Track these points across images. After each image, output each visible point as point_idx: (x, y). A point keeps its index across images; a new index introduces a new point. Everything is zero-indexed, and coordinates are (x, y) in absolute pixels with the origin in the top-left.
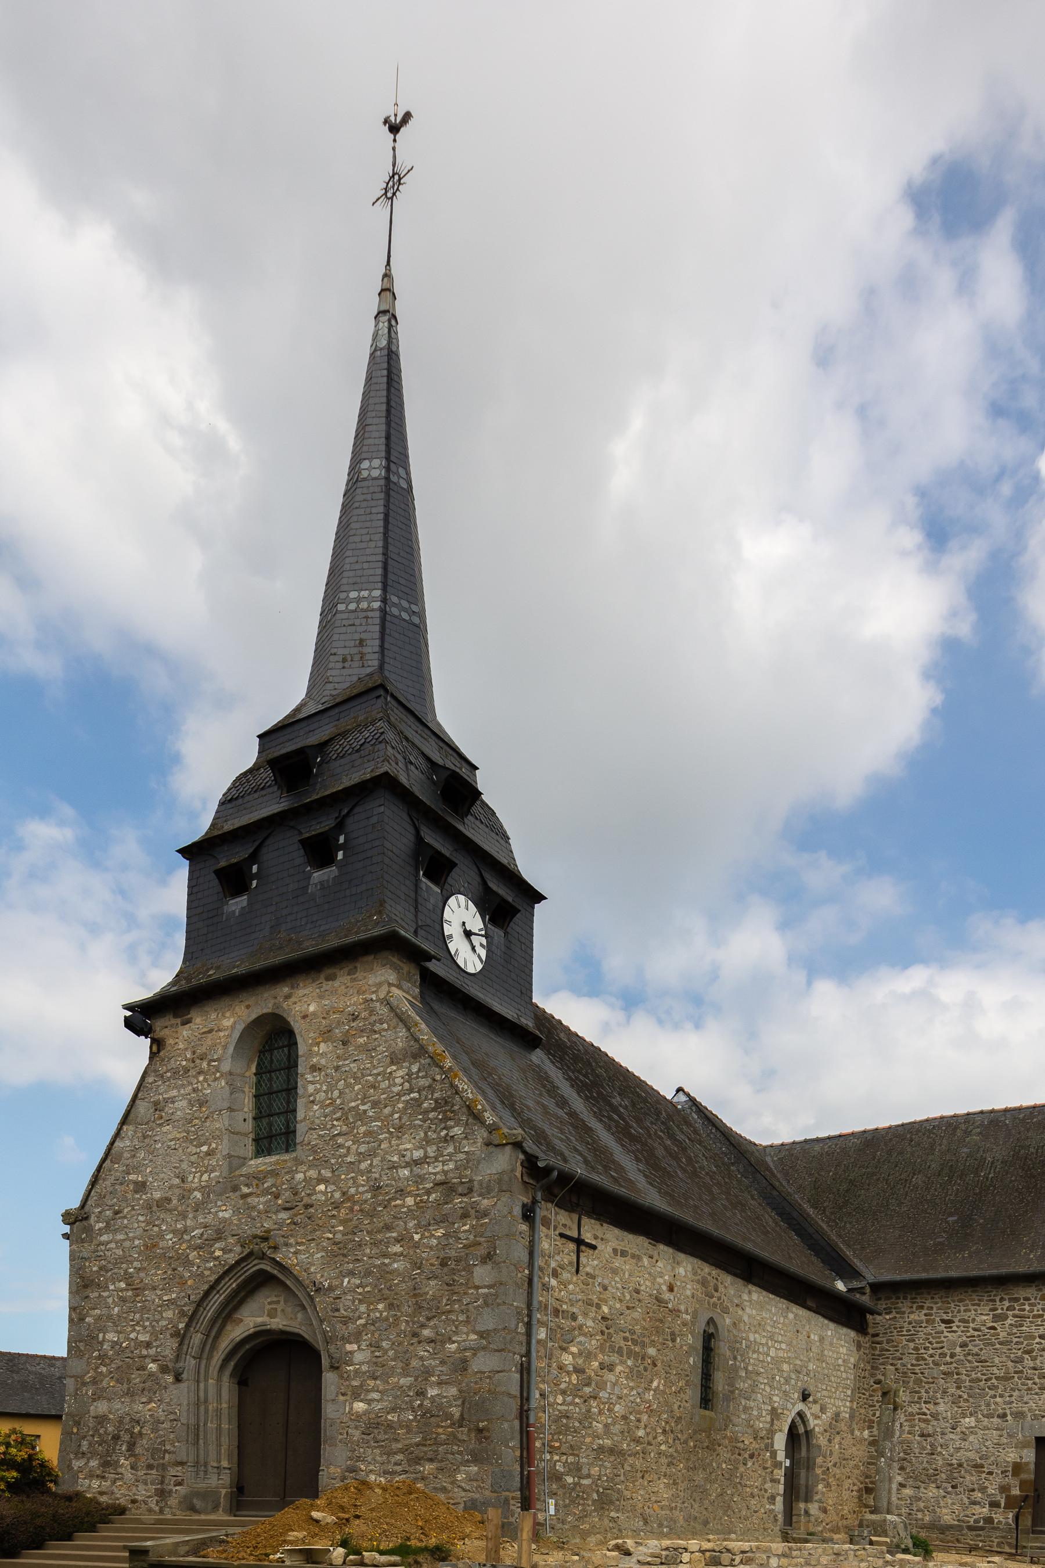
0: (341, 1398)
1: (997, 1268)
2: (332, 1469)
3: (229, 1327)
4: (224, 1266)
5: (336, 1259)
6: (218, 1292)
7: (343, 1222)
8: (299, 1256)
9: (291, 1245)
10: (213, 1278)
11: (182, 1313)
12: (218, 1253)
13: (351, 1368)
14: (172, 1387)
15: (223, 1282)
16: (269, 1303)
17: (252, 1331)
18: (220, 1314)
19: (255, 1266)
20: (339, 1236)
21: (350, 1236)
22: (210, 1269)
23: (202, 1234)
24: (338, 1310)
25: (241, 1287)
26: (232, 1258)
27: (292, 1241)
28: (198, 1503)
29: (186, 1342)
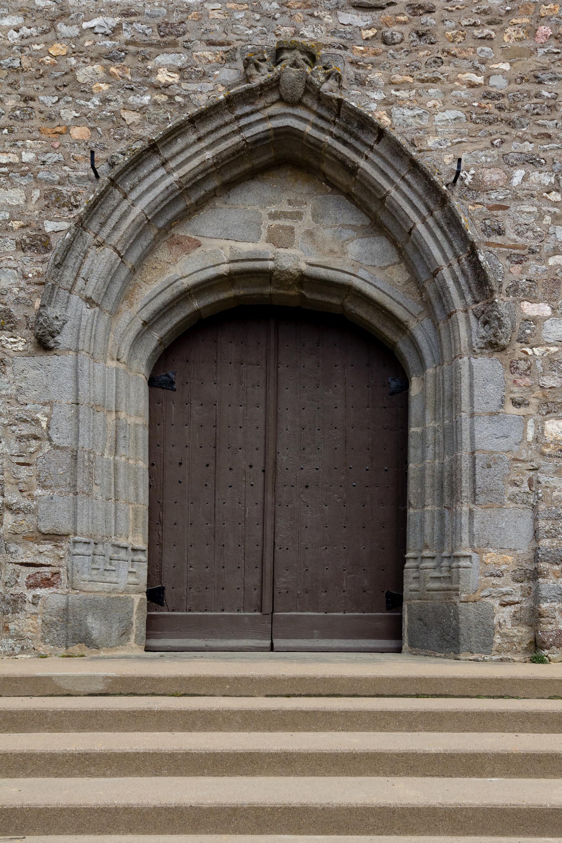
0: (511, 409)
1: (111, 485)
2: (491, 556)
3: (163, 254)
4: (182, 107)
5: (492, 129)
6: (164, 164)
7: (511, 55)
8: (395, 110)
9: (373, 85)
10: (151, 132)
11: (55, 200)
12: (163, 77)
13: (537, 351)
14: (21, 363)
15: (180, 143)
16: (274, 216)
17: (224, 269)
18: (157, 216)
19: (274, 117)
20: (498, 83)
21: (526, 86)
22: (142, 109)
23: (117, 29)
24: (500, 232)
25: (221, 164)
26: (204, 94)
27: (376, 75)
28: (95, 625)
29: (71, 262)
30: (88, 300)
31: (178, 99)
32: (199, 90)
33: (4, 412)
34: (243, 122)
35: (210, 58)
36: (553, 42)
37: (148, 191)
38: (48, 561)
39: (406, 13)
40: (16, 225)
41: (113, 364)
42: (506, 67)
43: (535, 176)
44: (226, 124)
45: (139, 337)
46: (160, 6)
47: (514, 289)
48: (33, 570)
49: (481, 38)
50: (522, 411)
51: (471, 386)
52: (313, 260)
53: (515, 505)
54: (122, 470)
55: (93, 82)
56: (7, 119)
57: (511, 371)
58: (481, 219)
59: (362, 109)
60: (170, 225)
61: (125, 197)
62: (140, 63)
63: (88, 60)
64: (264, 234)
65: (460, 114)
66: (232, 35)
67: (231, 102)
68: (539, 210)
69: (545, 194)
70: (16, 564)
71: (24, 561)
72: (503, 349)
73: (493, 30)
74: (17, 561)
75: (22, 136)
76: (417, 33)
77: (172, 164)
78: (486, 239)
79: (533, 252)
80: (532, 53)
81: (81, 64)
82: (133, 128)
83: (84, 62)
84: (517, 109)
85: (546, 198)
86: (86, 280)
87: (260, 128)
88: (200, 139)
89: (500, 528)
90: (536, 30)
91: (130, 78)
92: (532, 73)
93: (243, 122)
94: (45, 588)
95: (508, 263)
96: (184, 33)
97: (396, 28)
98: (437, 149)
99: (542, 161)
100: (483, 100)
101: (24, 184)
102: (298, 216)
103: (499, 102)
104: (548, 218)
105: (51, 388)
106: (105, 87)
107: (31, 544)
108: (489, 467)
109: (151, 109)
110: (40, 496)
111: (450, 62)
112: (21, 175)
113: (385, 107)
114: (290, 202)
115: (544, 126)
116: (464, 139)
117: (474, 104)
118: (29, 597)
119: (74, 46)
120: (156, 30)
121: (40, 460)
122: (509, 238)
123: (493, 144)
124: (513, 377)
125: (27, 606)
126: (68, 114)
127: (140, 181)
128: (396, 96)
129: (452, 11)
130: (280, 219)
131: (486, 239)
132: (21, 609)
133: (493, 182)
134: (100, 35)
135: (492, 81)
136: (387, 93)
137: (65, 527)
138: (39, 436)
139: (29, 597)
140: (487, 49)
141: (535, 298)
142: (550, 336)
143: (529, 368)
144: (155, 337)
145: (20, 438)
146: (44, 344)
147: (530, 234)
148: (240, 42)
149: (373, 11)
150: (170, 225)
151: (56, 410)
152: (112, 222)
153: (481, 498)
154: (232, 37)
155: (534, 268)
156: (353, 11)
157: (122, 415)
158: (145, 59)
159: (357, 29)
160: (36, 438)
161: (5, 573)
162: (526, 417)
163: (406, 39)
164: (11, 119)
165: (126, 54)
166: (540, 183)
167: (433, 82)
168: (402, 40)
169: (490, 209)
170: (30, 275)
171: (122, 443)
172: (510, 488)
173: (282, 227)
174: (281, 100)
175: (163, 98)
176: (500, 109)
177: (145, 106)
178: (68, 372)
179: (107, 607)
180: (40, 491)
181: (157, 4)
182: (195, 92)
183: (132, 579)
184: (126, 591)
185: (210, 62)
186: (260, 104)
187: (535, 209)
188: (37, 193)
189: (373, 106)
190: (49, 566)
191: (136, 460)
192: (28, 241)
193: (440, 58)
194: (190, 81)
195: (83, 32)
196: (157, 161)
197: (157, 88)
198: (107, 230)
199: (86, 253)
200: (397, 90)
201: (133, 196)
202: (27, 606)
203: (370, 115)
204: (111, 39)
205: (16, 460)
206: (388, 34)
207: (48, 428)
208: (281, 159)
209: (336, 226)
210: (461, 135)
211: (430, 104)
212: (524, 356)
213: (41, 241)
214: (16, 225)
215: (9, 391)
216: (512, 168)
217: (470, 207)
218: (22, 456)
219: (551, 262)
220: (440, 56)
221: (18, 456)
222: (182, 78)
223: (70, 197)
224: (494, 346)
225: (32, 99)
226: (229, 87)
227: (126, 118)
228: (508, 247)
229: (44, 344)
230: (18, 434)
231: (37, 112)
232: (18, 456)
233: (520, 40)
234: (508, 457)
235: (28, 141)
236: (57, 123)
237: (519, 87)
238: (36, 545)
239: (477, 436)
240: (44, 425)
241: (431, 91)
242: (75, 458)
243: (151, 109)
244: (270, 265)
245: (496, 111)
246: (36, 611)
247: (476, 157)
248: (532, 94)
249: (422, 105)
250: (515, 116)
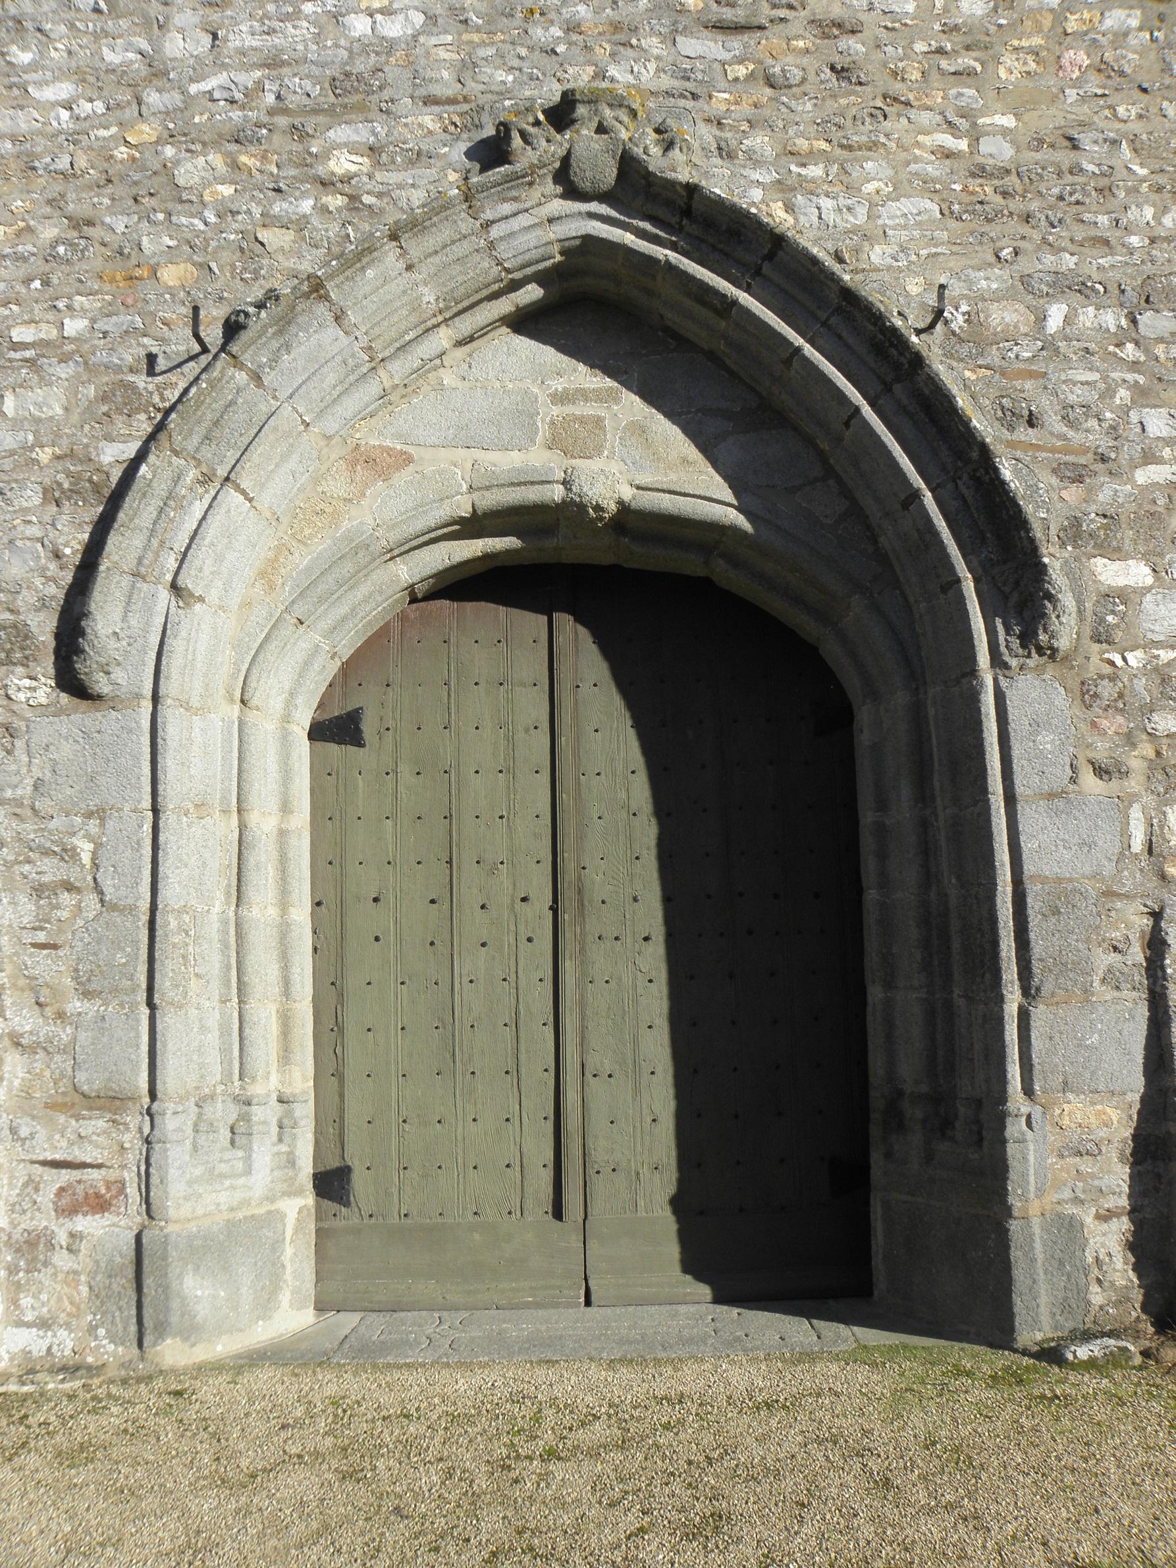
5: (993, 230)
9: (754, 160)
11: (119, 399)
12: (342, 164)
13: (1135, 659)
14: (44, 730)
22: (300, 224)
27: (759, 141)
31: (368, 199)
32: (411, 181)
33: (8, 836)
35: (431, 125)
36: (1094, 77)
39: (808, 35)
42: (1008, 121)
43: (1088, 316)
46: (337, 46)
47: (1074, 532)
48: (66, 1176)
49: (954, 74)
51: (1010, 799)
52: (645, 479)
53: (1116, 994)
55: (206, 184)
56: (41, 262)
57: (1083, 701)
58: (992, 397)
59: (736, 199)
62: (295, 144)
63: (199, 147)
66: (473, 84)
68: (1105, 378)
69: (1111, 348)
70: (33, 1162)
71: (49, 1156)
73: (976, 60)
74: (34, 1157)
75: (67, 290)
76: (833, 68)
78: (1006, 435)
79: (1103, 459)
80: (1054, 99)
81: (183, 154)
82: (280, 258)
83: (188, 151)
85: (1115, 355)
89: (1087, 1047)
90: (1059, 57)
91: (275, 171)
92: (1061, 132)
94: (94, 1214)
95: (1054, 481)
96: (381, 88)
97: (790, 59)
98: (889, 268)
99: (1098, 286)
100: (970, 180)
101: (63, 376)
103: (1001, 182)
104: (1123, 394)
105: (101, 780)
106: (227, 190)
107: (62, 1119)
108: (1056, 912)
109: (315, 221)
110: (80, 1014)
111: (899, 115)
112: (61, 361)
113: (780, 195)
116: (939, 250)
117: (953, 187)
118: (62, 1238)
119: (171, 126)
120: (327, 85)
121: (78, 935)
122: (1051, 433)
123: (998, 258)
124: (1090, 715)
128: (800, 175)
129: (893, 29)
130: (574, 403)
132: (46, 1264)
133: (1008, 325)
134: (222, 103)
136: (782, 171)
138: (77, 884)
139: (62, 1238)
140: (972, 92)
141: (1118, 549)
142: (1157, 628)
143: (1121, 695)
145: (39, 890)
148: (489, 96)
149: (742, 33)
151: (110, 824)
154: (473, 87)
156: (706, 32)
159: (716, 66)
160: (69, 887)
161: (10, 1184)
162: (1125, 802)
163: (812, 77)
164: (47, 261)
165: (270, 130)
167: (870, 149)
168: (804, 80)
170: (68, 551)
172: (1104, 957)
173: (582, 420)
176: (1005, 194)
177: (305, 216)
180: (78, 1004)
181: (329, 43)
182: (400, 186)
185: (430, 132)
189: (757, 194)
190: (99, 1166)
192: (66, 486)
193: (880, 108)
194: (392, 167)
197: (326, 184)
200: (804, 165)
203: (753, 210)
204: (243, 108)
205: (28, 938)
206: (777, 70)
207: (96, 866)
209: (690, 412)
212: (1107, 669)
213: (90, 481)
215: (19, 792)
216: (1041, 301)
217: (968, 374)
218: (42, 929)
220: (879, 103)
221: (34, 929)
222: (377, 164)
223: (152, 393)
225: (90, 223)
227: (265, 241)
228: (1053, 450)
230: (34, 880)
231: (97, 245)
232: (34, 929)
234: (1092, 889)
235: (78, 298)
236: (134, 261)
238: (73, 1122)
240: (86, 858)
241: (869, 165)
243: (315, 221)
245: (999, 199)
246: (75, 1266)
247: (970, 282)
248: (1065, 168)
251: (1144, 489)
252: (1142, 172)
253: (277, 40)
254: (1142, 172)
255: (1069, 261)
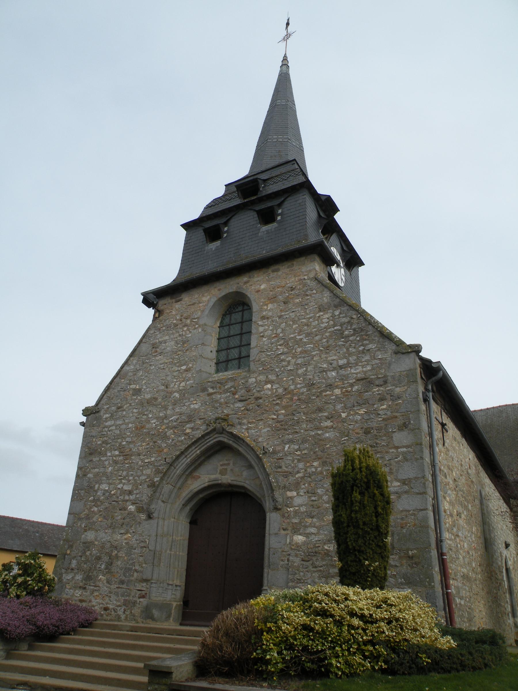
0: (283, 532)
3: (189, 482)
4: (192, 439)
6: (186, 457)
9: (244, 424)
10: (183, 448)
11: (158, 472)
12: (188, 431)
15: (190, 450)
17: (206, 485)
18: (185, 472)
20: (281, 417)
21: (290, 417)
23: (177, 419)
24: (280, 467)
25: (203, 453)
26: (198, 434)
27: (245, 421)
29: (159, 490)
30: (163, 501)
34: (207, 441)
36: (298, 401)
37: (181, 465)
38: (144, 589)
40: (148, 480)
41: (173, 520)
42: (283, 412)
44: (203, 442)
45: (181, 509)
48: (140, 592)
50: (286, 532)
51: (270, 524)
52: (232, 479)
54: (172, 556)
60: (191, 473)
61: (175, 468)
64: (219, 471)
65: (269, 429)
67: (203, 436)
72: (280, 509)
77: (188, 456)
79: (291, 473)
80: (291, 406)
84: (287, 425)
86: (163, 495)
87: (212, 442)
88: (196, 448)
93: (207, 441)
95: (283, 478)
102: (229, 464)
114: (226, 460)
115: (295, 429)
125: (137, 605)
126: (164, 445)
127: (179, 463)
131: (276, 470)
135: (279, 417)
137: (150, 578)
144: (188, 508)
146: (150, 517)
147: (290, 467)
150: (191, 473)
152: (171, 476)
153: (271, 567)
155: (291, 479)
157: (174, 537)
158: (183, 427)
160: (145, 547)
162: (287, 535)
166: (294, 449)
169: (278, 459)
171: (173, 546)
174: (217, 433)
175: (187, 437)
176: (282, 425)
178: (156, 525)
179: (164, 607)
183: (173, 596)
184: (170, 601)
186: (211, 435)
187: (291, 458)
188: (154, 470)
191: (179, 552)
195: (170, 421)
196: (184, 456)
197: (185, 434)
198: (169, 479)
199: (163, 487)
201: (177, 467)
202: (137, 605)
205: (139, 555)
208: (221, 448)
210: (270, 436)
211: (260, 427)
214: (148, 480)
219: (297, 476)
222: (192, 431)
224: (276, 509)
226: (204, 431)
229: (150, 517)
233: (288, 402)
234: (280, 550)
237: (287, 417)
239: (271, 542)
242: (154, 553)
244: (220, 482)
249: (258, 428)
250: (286, 427)
251: (297, 478)
252: (304, 418)
253: (182, 410)
254: (304, 418)
255: (291, 436)
